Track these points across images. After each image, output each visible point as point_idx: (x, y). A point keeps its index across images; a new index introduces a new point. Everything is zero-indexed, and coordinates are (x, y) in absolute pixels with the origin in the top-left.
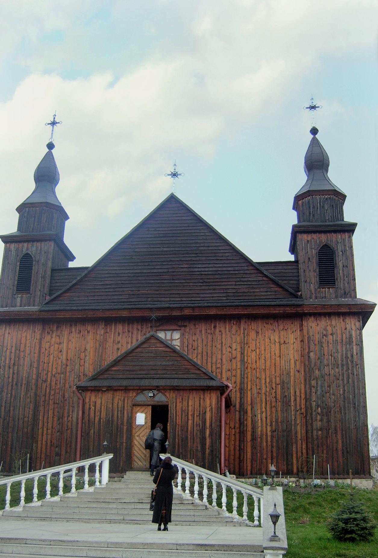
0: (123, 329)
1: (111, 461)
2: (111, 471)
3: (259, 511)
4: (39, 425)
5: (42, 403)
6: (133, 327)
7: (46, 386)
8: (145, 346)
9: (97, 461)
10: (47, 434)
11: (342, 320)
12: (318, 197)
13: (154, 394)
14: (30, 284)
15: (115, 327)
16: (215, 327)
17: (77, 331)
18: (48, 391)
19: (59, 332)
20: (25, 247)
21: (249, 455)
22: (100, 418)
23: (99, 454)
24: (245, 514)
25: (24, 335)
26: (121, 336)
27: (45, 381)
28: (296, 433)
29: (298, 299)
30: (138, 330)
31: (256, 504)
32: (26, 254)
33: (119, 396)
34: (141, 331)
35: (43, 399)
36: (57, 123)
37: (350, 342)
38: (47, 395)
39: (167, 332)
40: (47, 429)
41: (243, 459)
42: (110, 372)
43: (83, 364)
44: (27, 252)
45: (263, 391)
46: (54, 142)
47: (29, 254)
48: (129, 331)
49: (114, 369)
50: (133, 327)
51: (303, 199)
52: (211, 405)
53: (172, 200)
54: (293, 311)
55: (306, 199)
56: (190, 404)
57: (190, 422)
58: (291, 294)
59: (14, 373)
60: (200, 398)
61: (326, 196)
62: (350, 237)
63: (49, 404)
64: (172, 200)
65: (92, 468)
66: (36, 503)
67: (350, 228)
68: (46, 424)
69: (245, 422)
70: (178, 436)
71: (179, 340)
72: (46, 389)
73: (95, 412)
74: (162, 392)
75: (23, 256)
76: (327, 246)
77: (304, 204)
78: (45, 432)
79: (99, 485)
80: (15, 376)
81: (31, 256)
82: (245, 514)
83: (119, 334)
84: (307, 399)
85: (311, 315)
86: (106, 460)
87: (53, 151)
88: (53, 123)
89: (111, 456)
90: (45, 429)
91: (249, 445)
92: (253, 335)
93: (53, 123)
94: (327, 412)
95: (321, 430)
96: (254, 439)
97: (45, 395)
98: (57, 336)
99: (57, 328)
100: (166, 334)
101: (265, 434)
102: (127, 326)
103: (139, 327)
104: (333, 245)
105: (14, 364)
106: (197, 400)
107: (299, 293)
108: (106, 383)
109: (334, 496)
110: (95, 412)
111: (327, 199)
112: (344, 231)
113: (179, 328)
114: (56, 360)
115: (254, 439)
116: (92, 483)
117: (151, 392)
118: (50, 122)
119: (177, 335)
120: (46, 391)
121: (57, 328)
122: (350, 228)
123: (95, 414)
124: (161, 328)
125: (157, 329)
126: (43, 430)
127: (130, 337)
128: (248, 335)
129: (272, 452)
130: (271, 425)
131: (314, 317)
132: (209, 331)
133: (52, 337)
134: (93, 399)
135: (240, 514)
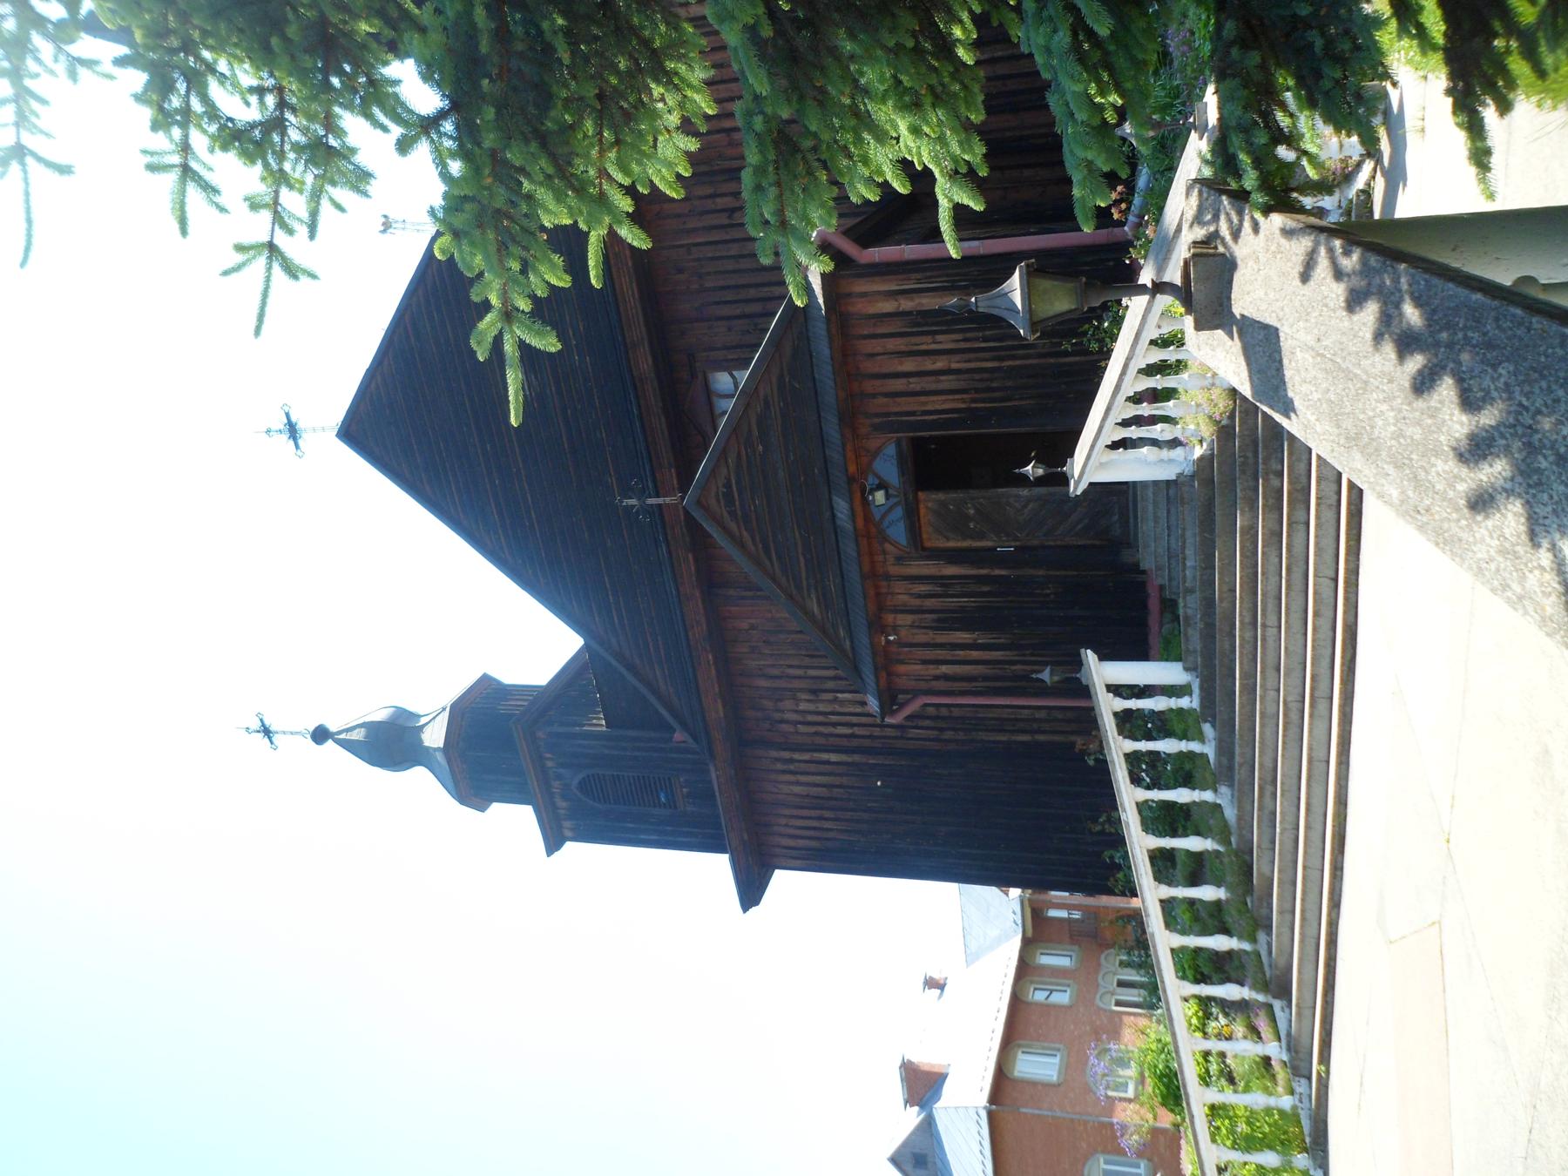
1: (1103, 657)
2: (1138, 652)
9: (1108, 706)
13: (879, 487)
14: (640, 805)
18: (927, 723)
23: (1085, 692)
36: (263, 725)
46: (311, 729)
47: (580, 783)
53: (358, 431)
64: (358, 431)
65: (1129, 723)
70: (1010, 399)
71: (734, 373)
74: (870, 463)
79: (1191, 695)
87: (333, 728)
88: (267, 732)
89: (1090, 656)
93: (267, 732)
97: (941, 730)
109: (1351, 375)
113: (700, 376)
117: (871, 498)
118: (266, 740)
119: (722, 381)
131: (149, 86)
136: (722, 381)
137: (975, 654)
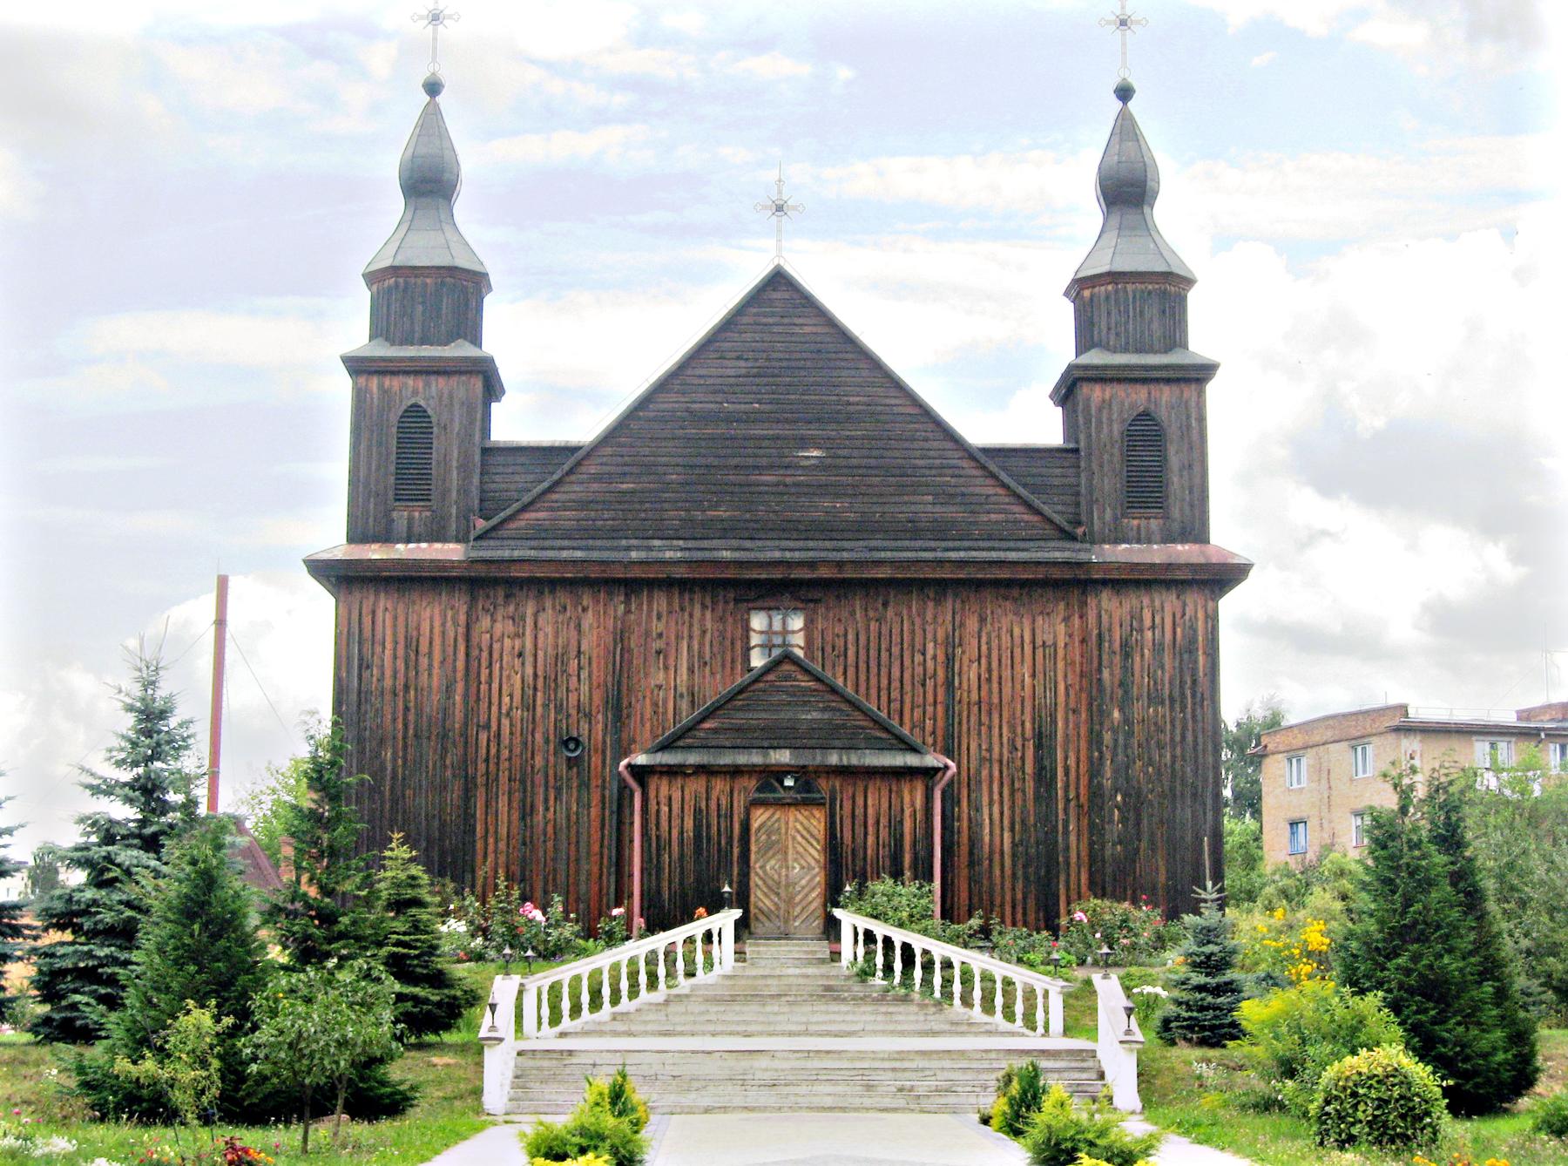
0: (670, 604)
3: (1046, 1012)
4: (474, 831)
5: (480, 780)
6: (691, 600)
7: (489, 740)
8: (771, 677)
10: (495, 852)
11: (1174, 596)
12: (1130, 287)
15: (648, 596)
16: (885, 605)
17: (558, 607)
19: (511, 608)
20: (410, 390)
21: (964, 895)
22: (682, 833)
24: (1019, 1017)
25: (428, 613)
26: (664, 620)
27: (487, 727)
28: (1067, 848)
29: (1078, 546)
30: (704, 607)
31: (1040, 1000)
32: (412, 406)
33: (720, 786)
34: (713, 610)
35: (482, 767)
37: (1191, 648)
38: (492, 761)
39: (773, 613)
40: (496, 842)
41: (952, 908)
42: (697, 733)
43: (576, 685)
44: (413, 401)
45: (996, 756)
48: (682, 609)
49: (706, 725)
50: (691, 600)
51: (1094, 287)
52: (913, 804)
53: (778, 280)
54: (1068, 575)
55: (1103, 288)
56: (870, 802)
57: (871, 840)
58: (1062, 530)
59: (407, 709)
60: (890, 791)
61: (1150, 287)
62: (1201, 394)
63: (497, 779)
65: (708, 937)
66: (625, 1004)
67: (1200, 374)
68: (491, 829)
69: (956, 824)
72: (488, 745)
73: (670, 817)
75: (406, 411)
76: (1148, 415)
77: (1095, 300)
78: (491, 848)
80: (411, 717)
81: (425, 411)
82: (1019, 1017)
83: (659, 618)
84: (1095, 771)
85: (1104, 583)
86: (727, 919)
89: (737, 913)
90: (491, 840)
91: (965, 872)
92: (972, 624)
94: (1135, 804)
95: (1120, 843)
96: (973, 863)
97: (487, 760)
98: (509, 617)
99: (507, 596)
100: (770, 618)
101: (998, 850)
102: (677, 595)
103: (708, 602)
104: (1163, 414)
105: (407, 687)
106: (885, 792)
107: (1080, 531)
108: (693, 758)
110: (670, 817)
111: (1150, 293)
112: (1187, 381)
114: (509, 677)
115: (973, 863)
116: (709, 964)
119: (797, 622)
120: (488, 751)
121: (507, 596)
122: (1200, 374)
123: (670, 821)
124: (759, 604)
125: (750, 605)
126: (486, 844)
127: (687, 624)
128: (962, 625)
129: (1013, 889)
130: (1012, 830)
132: (871, 614)
133: (494, 621)
134: (664, 791)
135: (1009, 1015)
136: (797, 622)
137: (675, 833)
